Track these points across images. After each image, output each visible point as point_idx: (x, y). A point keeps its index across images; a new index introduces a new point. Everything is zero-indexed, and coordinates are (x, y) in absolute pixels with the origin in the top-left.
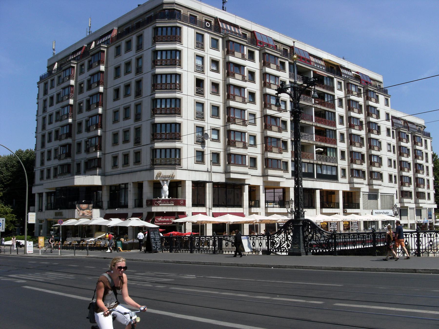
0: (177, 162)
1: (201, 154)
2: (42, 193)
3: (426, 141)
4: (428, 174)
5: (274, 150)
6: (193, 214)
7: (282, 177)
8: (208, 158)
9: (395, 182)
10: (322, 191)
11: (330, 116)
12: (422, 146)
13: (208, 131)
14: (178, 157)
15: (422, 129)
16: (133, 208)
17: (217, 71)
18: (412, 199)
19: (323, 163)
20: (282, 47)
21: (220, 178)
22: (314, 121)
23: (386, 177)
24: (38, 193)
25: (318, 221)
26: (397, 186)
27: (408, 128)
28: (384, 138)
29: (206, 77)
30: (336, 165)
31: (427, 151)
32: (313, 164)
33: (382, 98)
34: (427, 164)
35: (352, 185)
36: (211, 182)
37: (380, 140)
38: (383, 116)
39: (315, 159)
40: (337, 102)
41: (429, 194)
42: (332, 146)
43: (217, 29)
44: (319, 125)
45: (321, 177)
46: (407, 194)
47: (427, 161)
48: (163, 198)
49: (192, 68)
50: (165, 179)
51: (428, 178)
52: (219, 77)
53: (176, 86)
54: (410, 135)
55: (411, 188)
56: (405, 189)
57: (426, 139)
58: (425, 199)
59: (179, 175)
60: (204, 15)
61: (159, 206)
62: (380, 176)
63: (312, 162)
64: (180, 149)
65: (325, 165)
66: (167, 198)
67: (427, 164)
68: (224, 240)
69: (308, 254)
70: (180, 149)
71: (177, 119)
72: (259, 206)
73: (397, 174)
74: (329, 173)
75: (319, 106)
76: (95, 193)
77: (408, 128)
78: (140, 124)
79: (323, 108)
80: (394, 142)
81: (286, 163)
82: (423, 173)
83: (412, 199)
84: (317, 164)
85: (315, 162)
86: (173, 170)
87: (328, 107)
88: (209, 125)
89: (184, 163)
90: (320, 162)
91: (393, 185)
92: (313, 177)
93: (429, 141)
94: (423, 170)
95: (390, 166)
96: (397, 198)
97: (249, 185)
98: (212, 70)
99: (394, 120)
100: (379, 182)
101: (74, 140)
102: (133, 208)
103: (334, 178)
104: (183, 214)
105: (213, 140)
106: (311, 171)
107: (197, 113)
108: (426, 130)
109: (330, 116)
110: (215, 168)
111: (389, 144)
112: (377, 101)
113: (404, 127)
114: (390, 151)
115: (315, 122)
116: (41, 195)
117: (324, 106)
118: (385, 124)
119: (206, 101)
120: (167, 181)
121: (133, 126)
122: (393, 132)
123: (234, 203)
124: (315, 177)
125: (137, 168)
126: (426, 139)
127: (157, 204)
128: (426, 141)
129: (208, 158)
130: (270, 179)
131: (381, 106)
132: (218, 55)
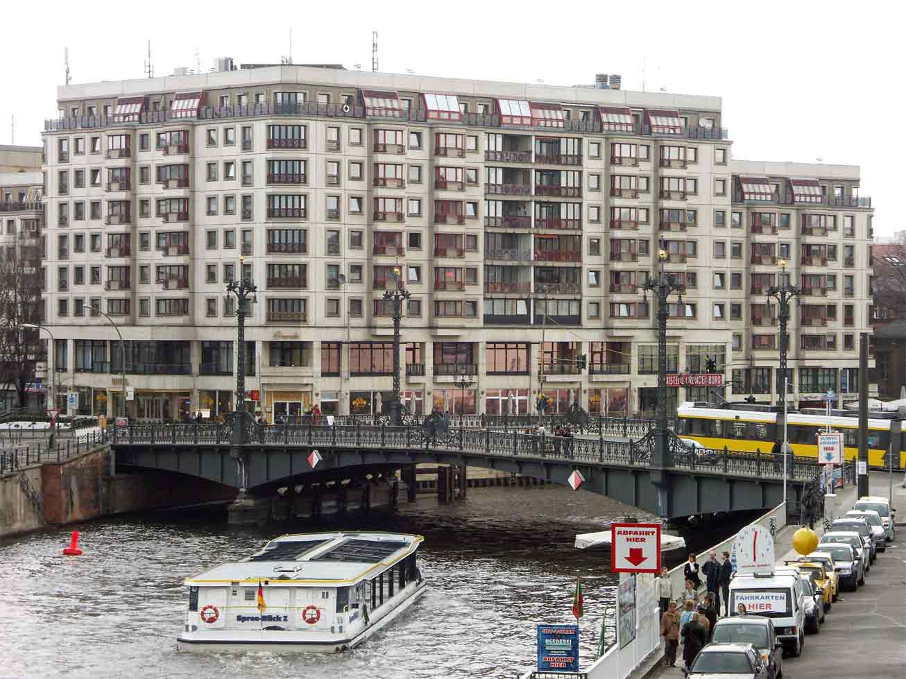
0: (302, 318)
1: (473, 271)
2: (65, 341)
8: (345, 307)
13: (344, 270)
14: (302, 311)
21: (358, 335)
24: (264, 342)
25: (325, 357)
29: (343, 158)
30: (578, 297)
35: (433, 332)
49: (322, 181)
53: (300, 212)
59: (305, 335)
60: (340, 90)
64: (305, 300)
68: (15, 238)
70: (305, 300)
71: (302, 259)
72: (423, 374)
74: (563, 312)
88: (347, 261)
89: (312, 319)
92: (529, 322)
101: (134, 161)
105: (352, 281)
110: (355, 322)
116: (60, 344)
119: (342, 227)
123: (372, 366)
124: (532, 322)
130: (440, 332)
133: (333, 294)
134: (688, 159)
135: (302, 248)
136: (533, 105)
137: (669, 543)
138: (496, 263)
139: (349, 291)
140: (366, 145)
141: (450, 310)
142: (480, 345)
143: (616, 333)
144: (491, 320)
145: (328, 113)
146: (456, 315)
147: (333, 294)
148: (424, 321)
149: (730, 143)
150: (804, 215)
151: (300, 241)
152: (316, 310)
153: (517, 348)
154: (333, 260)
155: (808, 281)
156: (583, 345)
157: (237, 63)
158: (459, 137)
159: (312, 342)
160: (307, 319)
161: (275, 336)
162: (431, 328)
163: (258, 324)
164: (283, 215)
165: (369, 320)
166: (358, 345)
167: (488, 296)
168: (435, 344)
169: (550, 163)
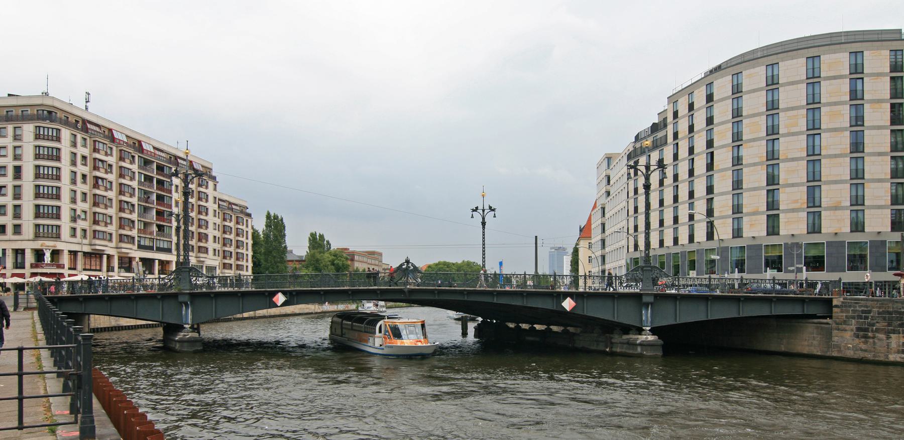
3: (247, 220)
4: (247, 250)
5: (127, 228)
6: (70, 275)
7: (106, 246)
8: (79, 233)
9: (219, 256)
10: (160, 260)
11: (168, 199)
12: (243, 224)
15: (244, 210)
16: (12, 269)
17: (85, 165)
18: (232, 270)
19: (161, 239)
20: (132, 141)
21: (87, 249)
22: (155, 204)
23: (211, 252)
26: (220, 258)
27: (232, 209)
28: (211, 218)
31: (247, 230)
32: (154, 239)
33: (211, 184)
34: (247, 241)
36: (82, 252)
37: (208, 220)
38: (211, 199)
39: (155, 235)
40: (174, 188)
41: (247, 266)
42: (169, 225)
43: (85, 130)
44: (159, 208)
45: (160, 250)
46: (149, 179)
47: (247, 238)
48: (46, 262)
50: (48, 248)
51: (247, 253)
52: (86, 170)
54: (233, 216)
55: (232, 261)
56: (226, 261)
57: (247, 219)
58: (244, 271)
59: (59, 246)
60: (74, 116)
61: (43, 268)
62: (206, 250)
63: (153, 237)
65: (162, 240)
66: (49, 262)
67: (247, 241)
69: (60, 379)
73: (220, 223)
74: (166, 247)
75: (160, 192)
76: (181, 261)
77: (232, 209)
78: (21, 202)
79: (163, 193)
80: (218, 221)
81: (111, 234)
82: (243, 249)
83: (232, 270)
84: (156, 239)
85: (155, 238)
86: (55, 242)
87: (166, 193)
90: (158, 238)
91: (216, 258)
93: (250, 220)
94: (243, 246)
95: (215, 242)
96: (219, 269)
97: (107, 254)
98: (83, 164)
99: (220, 203)
100: (205, 255)
102: (12, 269)
103: (169, 251)
104: (62, 275)
106: (151, 244)
107: (72, 198)
108: (248, 211)
109: (168, 199)
110: (86, 241)
111: (215, 224)
112: (207, 187)
113: (229, 208)
114: (215, 229)
115: (157, 205)
117: (164, 192)
118: (211, 206)
120: (49, 249)
121: (11, 203)
122: (219, 213)
125: (17, 237)
126: (247, 219)
127: (42, 266)
128: (247, 220)
129: (79, 233)
131: (210, 191)
132: (86, 152)
133: (73, 225)
134: (45, 134)
135: (58, 197)
136: (155, 148)
137: (879, 233)
138: (142, 219)
139: (81, 224)
140: (88, 147)
141: (101, 236)
142: (65, 251)
143: (98, 247)
144: (140, 247)
145: (74, 126)
146: (103, 239)
147: (73, 225)
148: (113, 244)
149: (218, 182)
150: (237, 217)
151: (57, 193)
152: (65, 233)
153: (96, 257)
154: (74, 206)
155: (123, 222)
156: (26, 251)
157: (88, 104)
158: (105, 145)
159: (63, 250)
160: (61, 237)
161: (42, 245)
162: (91, 245)
163: (27, 238)
164: (46, 177)
165: (90, 241)
166: (86, 254)
167: (139, 235)
168: (119, 257)
169: (143, 170)
